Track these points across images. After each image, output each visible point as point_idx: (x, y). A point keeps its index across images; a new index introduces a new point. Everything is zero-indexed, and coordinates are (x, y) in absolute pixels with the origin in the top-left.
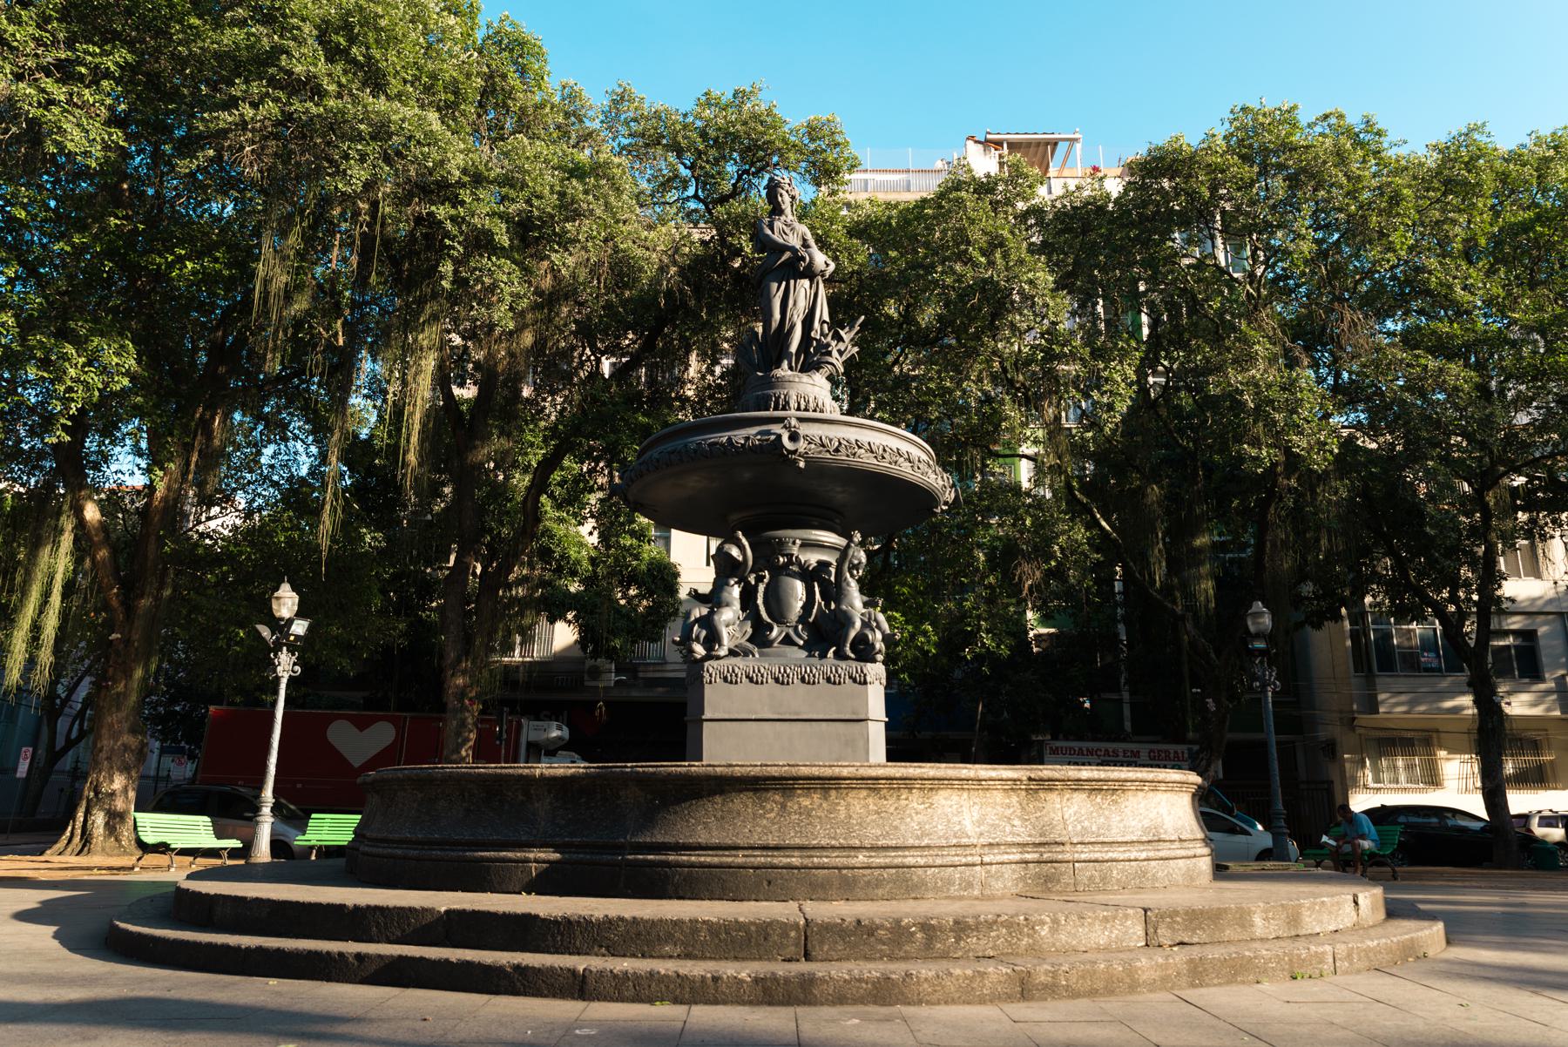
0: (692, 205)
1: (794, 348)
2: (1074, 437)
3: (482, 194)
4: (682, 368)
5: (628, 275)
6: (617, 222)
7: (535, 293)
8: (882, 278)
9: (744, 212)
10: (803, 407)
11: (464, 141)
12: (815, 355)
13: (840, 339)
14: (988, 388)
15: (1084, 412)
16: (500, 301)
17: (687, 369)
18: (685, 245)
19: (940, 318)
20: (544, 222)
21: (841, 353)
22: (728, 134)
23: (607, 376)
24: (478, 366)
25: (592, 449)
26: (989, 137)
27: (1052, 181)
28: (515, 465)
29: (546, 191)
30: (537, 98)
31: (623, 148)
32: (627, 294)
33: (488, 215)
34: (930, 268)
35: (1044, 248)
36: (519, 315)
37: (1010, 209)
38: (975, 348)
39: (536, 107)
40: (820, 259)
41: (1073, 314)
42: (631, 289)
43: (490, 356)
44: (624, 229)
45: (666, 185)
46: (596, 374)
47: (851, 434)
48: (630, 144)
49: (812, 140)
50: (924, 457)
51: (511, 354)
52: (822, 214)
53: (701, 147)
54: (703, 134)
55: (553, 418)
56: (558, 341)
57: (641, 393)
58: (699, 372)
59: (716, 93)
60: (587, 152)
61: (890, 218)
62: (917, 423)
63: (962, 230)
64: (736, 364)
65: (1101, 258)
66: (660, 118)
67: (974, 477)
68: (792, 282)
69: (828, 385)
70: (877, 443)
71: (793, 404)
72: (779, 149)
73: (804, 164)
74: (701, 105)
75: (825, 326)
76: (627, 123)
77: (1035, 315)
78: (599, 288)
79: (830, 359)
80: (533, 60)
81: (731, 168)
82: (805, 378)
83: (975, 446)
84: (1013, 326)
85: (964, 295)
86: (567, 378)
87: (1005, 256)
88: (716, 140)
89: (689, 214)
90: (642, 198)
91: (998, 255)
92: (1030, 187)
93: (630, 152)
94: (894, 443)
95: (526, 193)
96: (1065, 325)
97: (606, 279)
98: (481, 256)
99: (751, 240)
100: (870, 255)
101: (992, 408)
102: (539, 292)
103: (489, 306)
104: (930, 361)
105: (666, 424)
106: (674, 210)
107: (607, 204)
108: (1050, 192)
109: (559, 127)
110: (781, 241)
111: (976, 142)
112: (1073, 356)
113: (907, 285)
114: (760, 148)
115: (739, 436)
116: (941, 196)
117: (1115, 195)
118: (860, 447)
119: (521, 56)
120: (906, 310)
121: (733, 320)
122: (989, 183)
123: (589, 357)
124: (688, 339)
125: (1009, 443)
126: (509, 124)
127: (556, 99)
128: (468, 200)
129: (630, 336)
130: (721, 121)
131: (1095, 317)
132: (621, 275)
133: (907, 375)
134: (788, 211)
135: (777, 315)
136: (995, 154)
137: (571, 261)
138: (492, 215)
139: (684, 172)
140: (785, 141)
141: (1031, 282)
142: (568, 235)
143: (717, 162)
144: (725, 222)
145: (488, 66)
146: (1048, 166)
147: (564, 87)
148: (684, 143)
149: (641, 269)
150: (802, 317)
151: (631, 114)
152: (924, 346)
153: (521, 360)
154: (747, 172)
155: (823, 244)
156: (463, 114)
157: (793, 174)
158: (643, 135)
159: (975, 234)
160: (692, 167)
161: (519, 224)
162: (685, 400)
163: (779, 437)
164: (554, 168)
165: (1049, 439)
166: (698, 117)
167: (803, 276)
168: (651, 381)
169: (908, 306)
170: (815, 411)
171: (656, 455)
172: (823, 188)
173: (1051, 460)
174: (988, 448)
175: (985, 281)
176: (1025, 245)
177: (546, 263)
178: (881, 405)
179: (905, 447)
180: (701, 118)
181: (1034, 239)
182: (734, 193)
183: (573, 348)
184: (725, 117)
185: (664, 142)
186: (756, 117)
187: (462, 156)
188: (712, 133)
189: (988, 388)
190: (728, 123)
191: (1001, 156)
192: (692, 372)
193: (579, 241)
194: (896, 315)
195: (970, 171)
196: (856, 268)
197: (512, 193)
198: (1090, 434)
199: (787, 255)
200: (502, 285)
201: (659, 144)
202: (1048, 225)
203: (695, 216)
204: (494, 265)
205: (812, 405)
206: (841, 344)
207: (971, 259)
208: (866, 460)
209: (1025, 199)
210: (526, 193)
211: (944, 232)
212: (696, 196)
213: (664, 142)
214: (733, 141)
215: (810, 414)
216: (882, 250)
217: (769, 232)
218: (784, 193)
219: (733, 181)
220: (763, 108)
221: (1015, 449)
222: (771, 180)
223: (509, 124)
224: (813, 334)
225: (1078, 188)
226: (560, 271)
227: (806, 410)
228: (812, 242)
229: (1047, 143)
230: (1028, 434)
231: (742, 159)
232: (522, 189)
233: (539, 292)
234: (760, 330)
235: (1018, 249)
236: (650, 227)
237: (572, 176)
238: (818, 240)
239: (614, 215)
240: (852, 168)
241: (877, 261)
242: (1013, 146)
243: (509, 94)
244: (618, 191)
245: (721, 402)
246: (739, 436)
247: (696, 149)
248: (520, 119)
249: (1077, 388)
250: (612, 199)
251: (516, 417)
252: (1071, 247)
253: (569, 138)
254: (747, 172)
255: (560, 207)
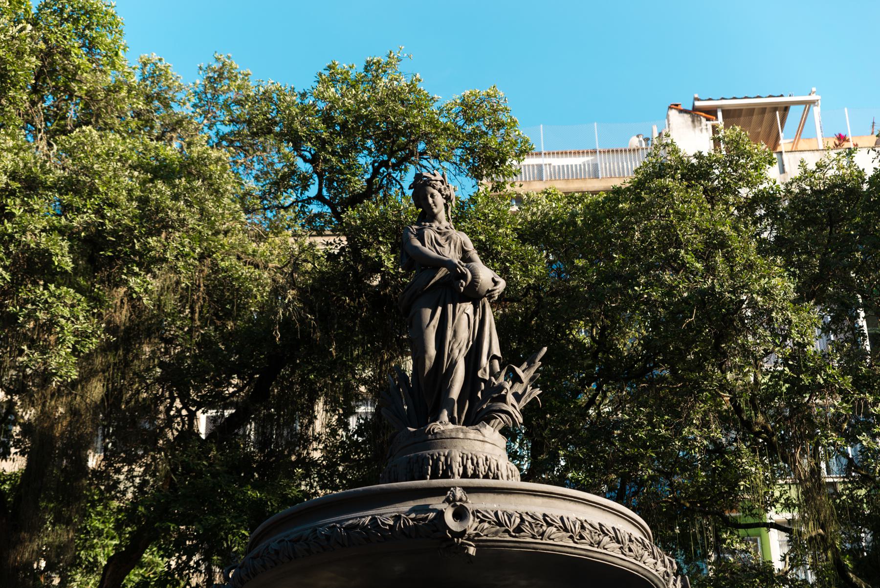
0: (315, 208)
1: (455, 393)
2: (840, 495)
3: (36, 203)
4: (306, 421)
5: (231, 302)
6: (217, 233)
7: (107, 330)
8: (571, 295)
9: (383, 215)
10: (470, 472)
11: (13, 137)
12: (484, 400)
13: (517, 379)
14: (718, 434)
15: (851, 461)
16: (60, 341)
17: (311, 422)
18: (306, 261)
19: (647, 343)
20: (120, 238)
21: (518, 397)
22: (358, 118)
23: (203, 437)
24: (27, 428)
25: (183, 537)
26: (698, 104)
27: (785, 156)
28: (75, 563)
29: (123, 197)
30: (110, 79)
31: (223, 138)
32: (230, 325)
33: (44, 230)
34: (630, 280)
35: (780, 246)
36: (84, 360)
37: (731, 199)
38: (696, 382)
39: (108, 91)
40: (486, 275)
41: (826, 329)
42: (235, 320)
43: (44, 415)
44: (225, 241)
45: (281, 183)
46: (189, 433)
47: (537, 507)
48: (231, 133)
49: (469, 121)
50: (637, 534)
51: (73, 412)
52: (484, 215)
53: (325, 135)
54: (328, 119)
55: (129, 495)
56: (138, 392)
57: (249, 457)
58: (328, 425)
59: (342, 65)
60: (176, 144)
61: (574, 215)
62: (623, 484)
63: (670, 227)
64: (377, 414)
65: (858, 255)
66: (271, 99)
67: (706, 556)
68: (450, 307)
69: (502, 441)
70: (573, 517)
71: (457, 468)
72: (426, 134)
73: (459, 152)
74: (324, 82)
75: (496, 362)
76: (227, 106)
77: (774, 335)
78: (192, 319)
79: (505, 407)
80: (104, 32)
81: (364, 160)
82: (472, 433)
83: (705, 514)
84: (746, 352)
85: (678, 310)
86: (150, 440)
87: (729, 258)
88: (344, 125)
89: (311, 220)
90: (249, 200)
91: (719, 259)
92: (755, 168)
93: (231, 143)
94: (595, 517)
95: (96, 201)
96: (817, 345)
97: (202, 306)
98: (35, 284)
99: (393, 251)
100: (550, 263)
101: (726, 462)
102: (111, 329)
103: (44, 351)
104: (636, 399)
105: (285, 501)
106: (291, 214)
107: (202, 211)
108: (783, 171)
109: (138, 114)
110: (434, 254)
111: (682, 111)
112: (828, 388)
113: (600, 302)
114: (401, 133)
115: (387, 514)
116: (640, 185)
117: (869, 173)
118: (549, 525)
119: (88, 27)
120: (602, 334)
121: (372, 356)
122: (700, 165)
123: (179, 411)
124: (313, 383)
125: (751, 509)
126: (73, 112)
127: (135, 79)
128: (18, 212)
129: (235, 381)
130: (349, 102)
131: (857, 332)
132: (221, 301)
133: (607, 422)
134: (442, 215)
135: (432, 351)
136: (706, 125)
137: (155, 285)
138: (50, 230)
139: (304, 167)
140: (432, 123)
141: (765, 292)
142: (153, 253)
143: (346, 151)
144: (358, 229)
145: (45, 41)
146: (778, 138)
147: (145, 64)
148: (302, 131)
149: (249, 294)
150: (464, 352)
151: (232, 95)
152: (627, 380)
153: (87, 417)
154: (385, 164)
155: (488, 253)
156: (12, 102)
157: (446, 165)
158: (249, 122)
159: (686, 232)
160: (314, 161)
161: (86, 240)
162: (309, 464)
163: (441, 514)
164: (133, 167)
165: (806, 501)
166: (321, 97)
167: (464, 299)
168: (263, 442)
169: (604, 328)
170: (486, 477)
171: (274, 545)
172: (484, 181)
173: (810, 531)
174: (721, 514)
175: (703, 292)
176: (753, 244)
177: (122, 290)
178: (574, 462)
179: (610, 521)
180: (324, 99)
181: (765, 235)
182: (370, 191)
183: (158, 399)
184: (355, 96)
185: (277, 129)
186: (394, 94)
187: (10, 156)
188: (339, 117)
189: (718, 434)
190: (358, 103)
191: (715, 130)
192: (318, 426)
193: (165, 260)
194: (587, 341)
195: (675, 151)
196: (532, 282)
197: (77, 201)
198: (862, 492)
199: (442, 272)
200: (63, 321)
201: (270, 132)
202: (783, 215)
203: (318, 223)
204: (52, 295)
205: (482, 469)
206: (517, 385)
207: (683, 265)
208: (560, 541)
209: (750, 184)
210: (96, 201)
211: (645, 231)
212: (319, 197)
213: (277, 129)
214: (366, 126)
215: (480, 482)
216: (567, 257)
217: (418, 244)
218: (436, 192)
219: (367, 176)
220: (403, 83)
221: (760, 517)
222: (418, 177)
223: (73, 112)
224: (480, 374)
225: (820, 166)
226: (140, 299)
227: (475, 475)
228: (474, 254)
229: (774, 108)
230: (777, 494)
231: (379, 148)
232: (90, 196)
233: (111, 329)
234: (408, 365)
235: (746, 250)
236: (259, 238)
237: (155, 177)
238: (481, 248)
239: (211, 225)
240: (523, 153)
241: (559, 272)
242: (731, 115)
243: (72, 76)
244: (217, 193)
245: (358, 464)
246: (387, 514)
247: (319, 138)
248: (87, 106)
249: (838, 430)
250: (210, 205)
251: (79, 498)
252: (815, 244)
253: (152, 128)
254: (385, 164)
255: (141, 217)
